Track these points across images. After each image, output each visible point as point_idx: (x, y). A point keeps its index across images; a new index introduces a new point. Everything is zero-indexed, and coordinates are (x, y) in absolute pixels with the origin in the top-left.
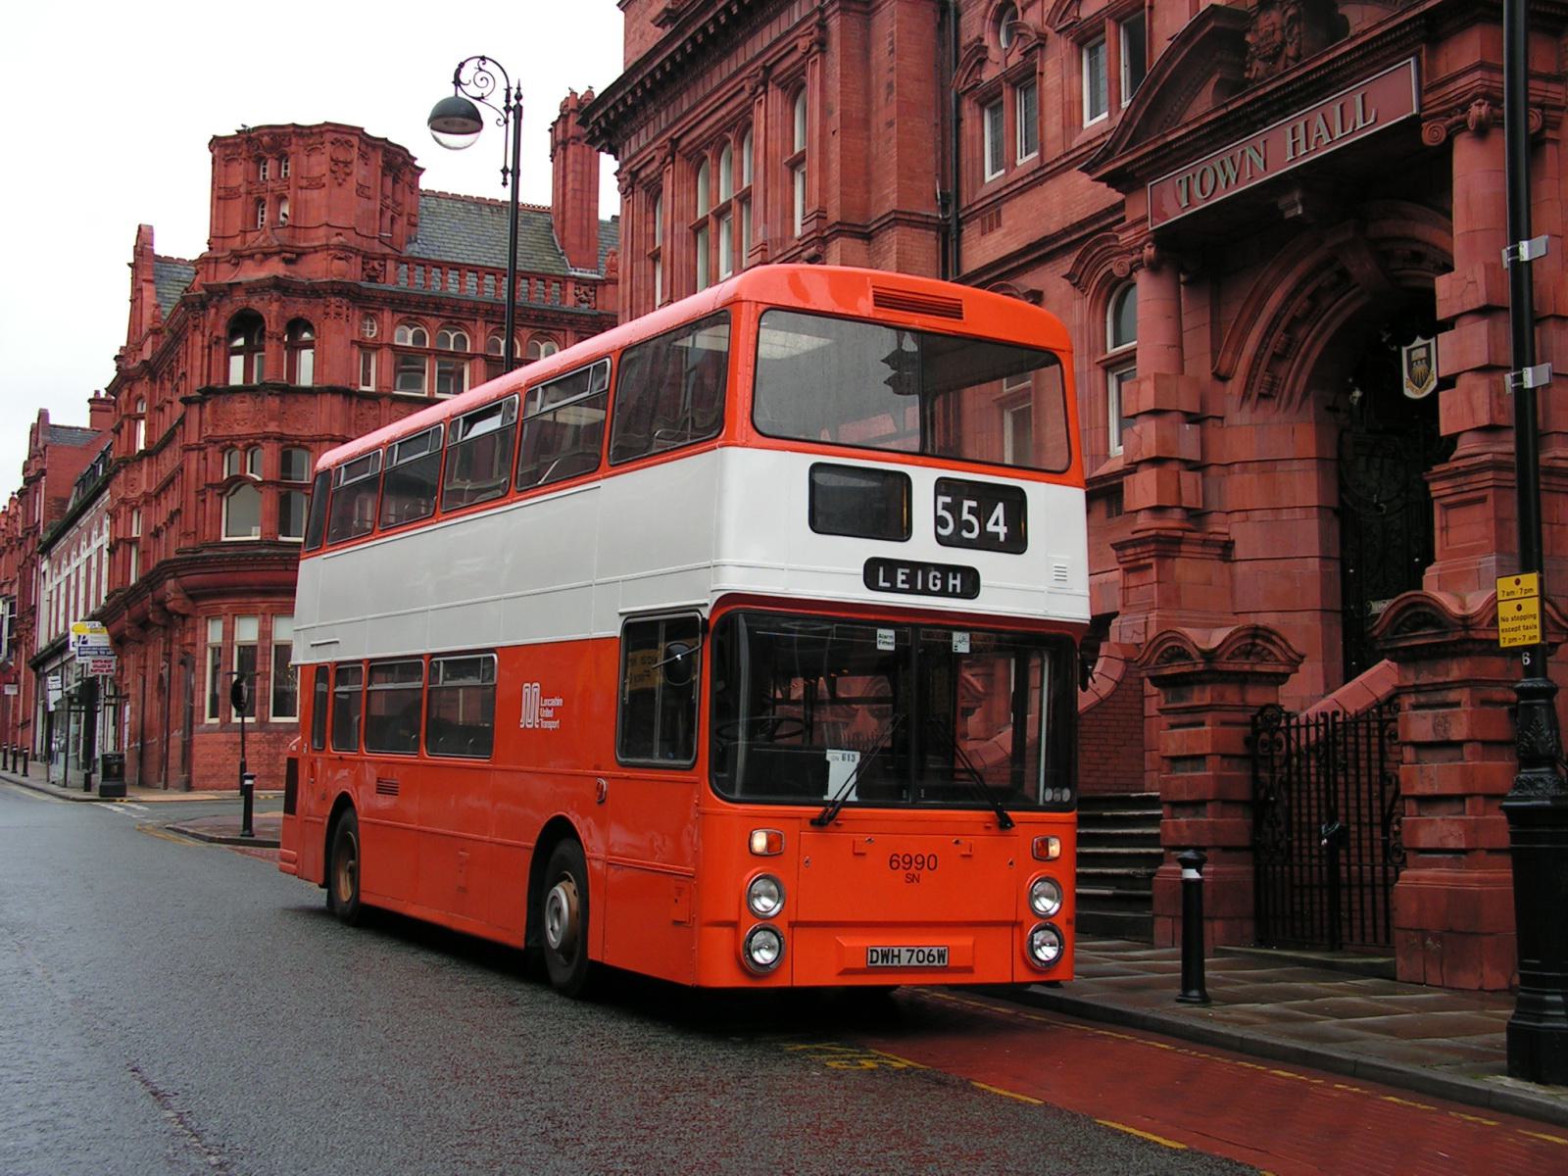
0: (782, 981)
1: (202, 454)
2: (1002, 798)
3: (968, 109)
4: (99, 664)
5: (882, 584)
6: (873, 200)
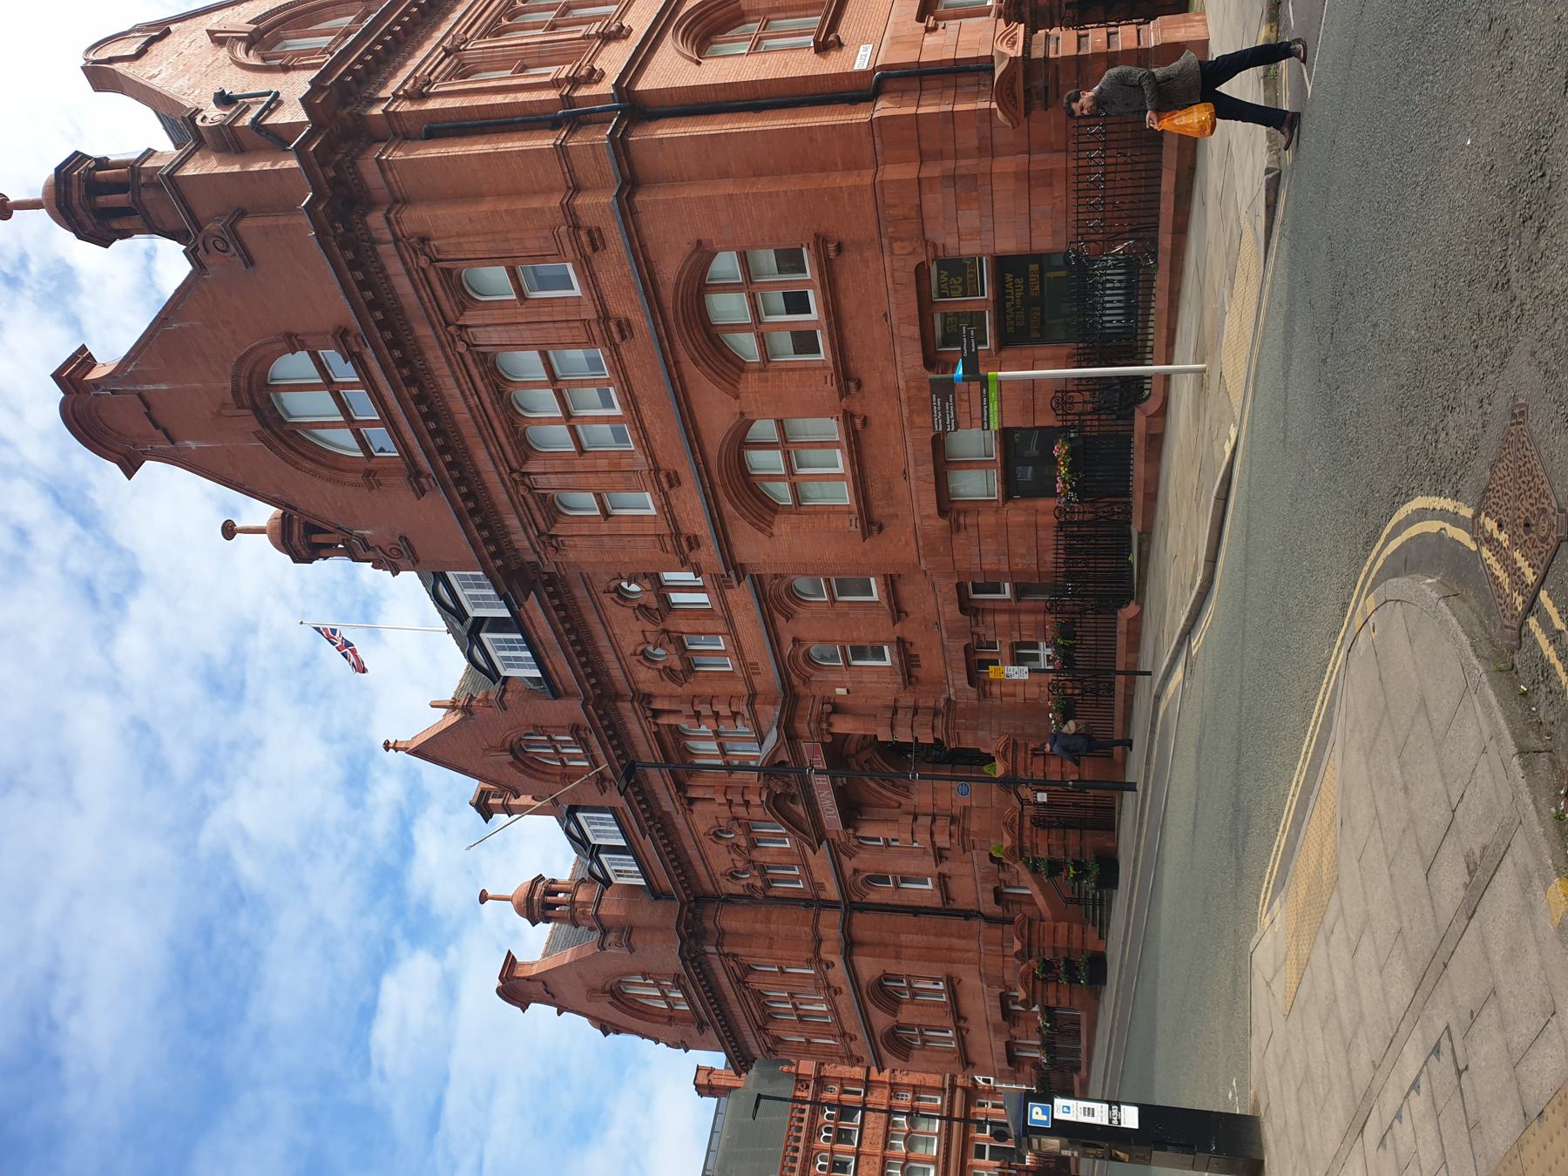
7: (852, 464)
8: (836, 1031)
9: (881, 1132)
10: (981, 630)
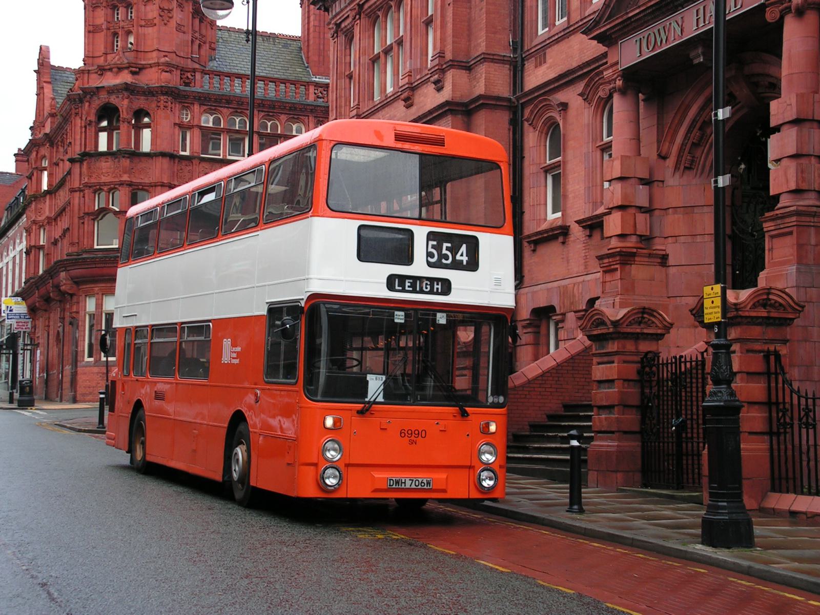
0: (341, 494)
1: (82, 194)
2: (463, 402)
4: (20, 324)
5: (397, 288)
6: (473, 45)
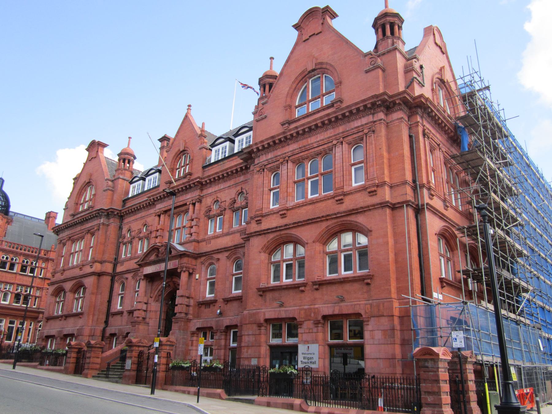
3: (121, 245)
7: (287, 285)
8: (66, 268)
9: (25, 283)
10: (218, 334)
